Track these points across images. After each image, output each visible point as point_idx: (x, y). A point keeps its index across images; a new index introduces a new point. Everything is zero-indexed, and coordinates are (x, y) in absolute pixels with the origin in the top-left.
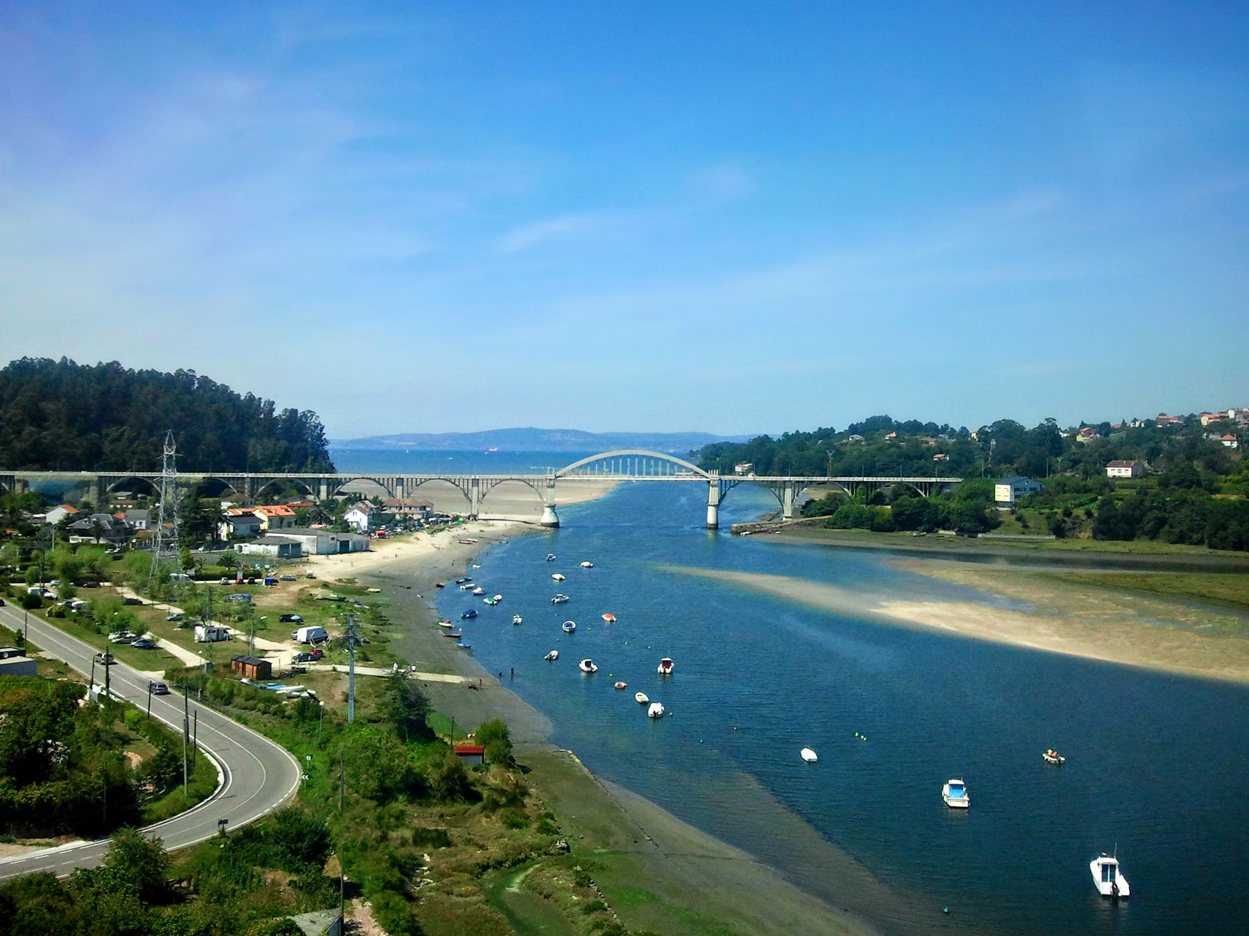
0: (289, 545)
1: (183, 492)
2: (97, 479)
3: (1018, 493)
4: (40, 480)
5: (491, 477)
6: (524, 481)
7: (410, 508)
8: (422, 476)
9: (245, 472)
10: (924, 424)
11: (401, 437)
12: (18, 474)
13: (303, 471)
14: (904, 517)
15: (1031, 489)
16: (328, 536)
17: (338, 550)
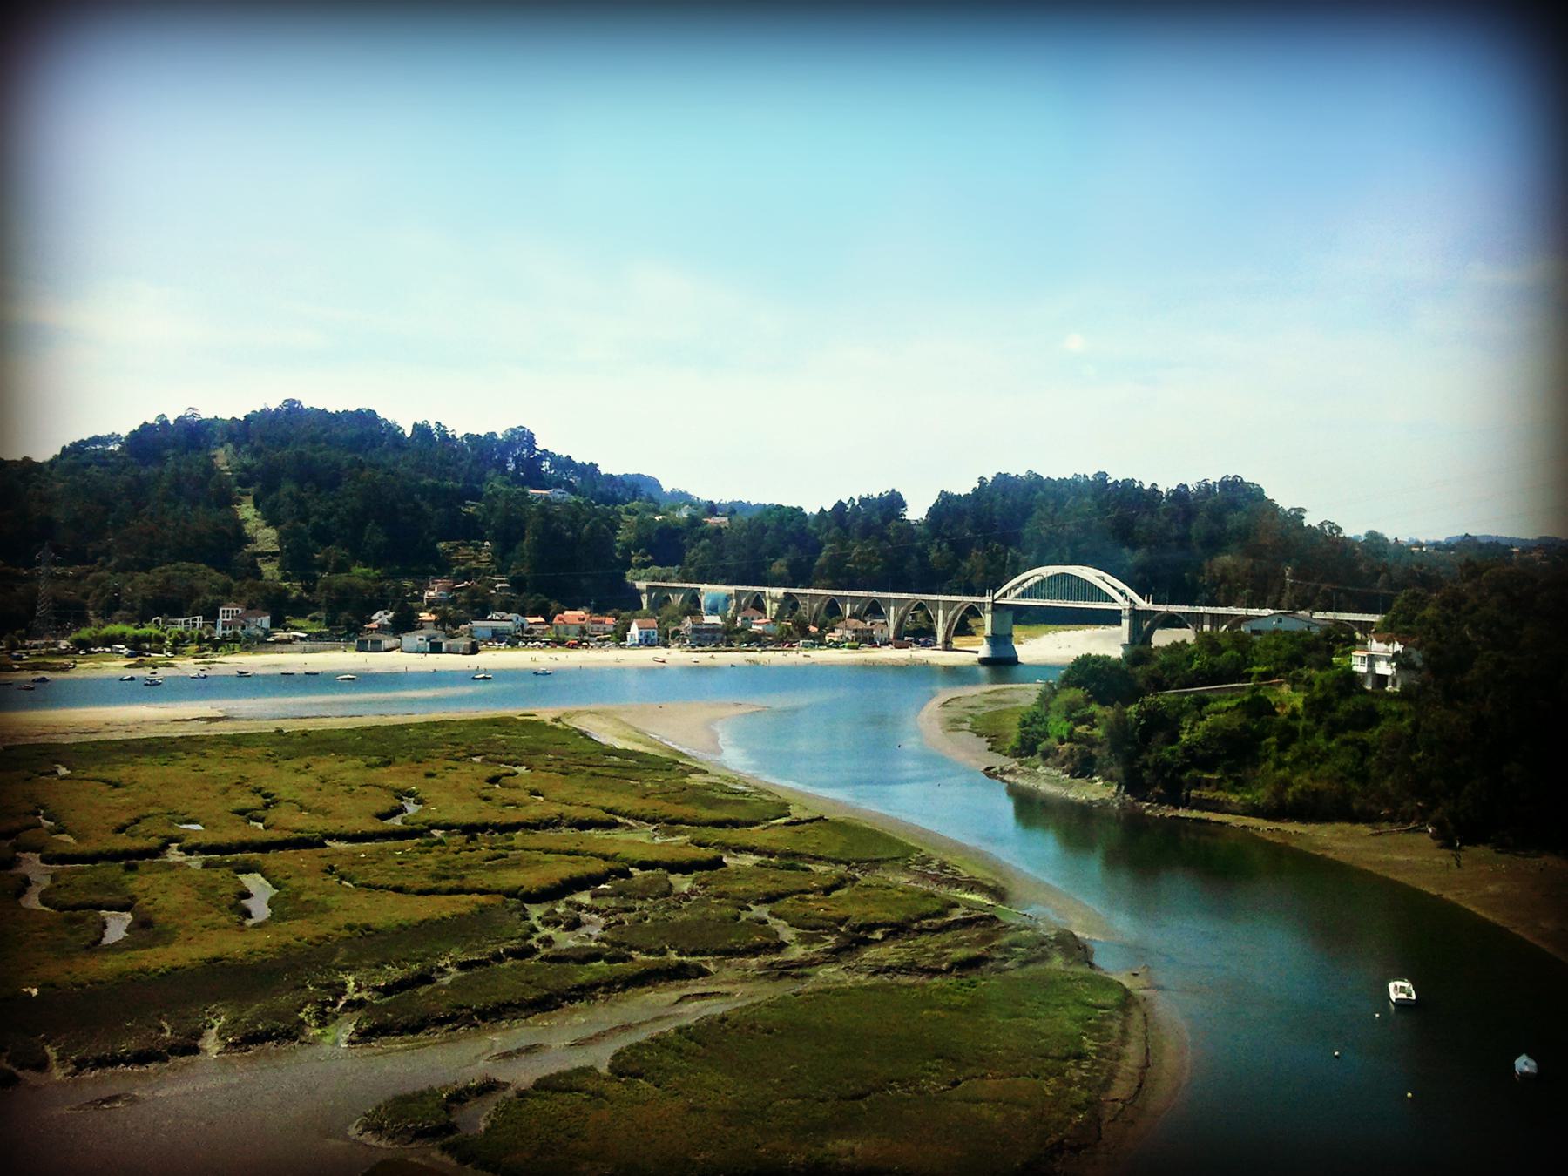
17: (428, 649)
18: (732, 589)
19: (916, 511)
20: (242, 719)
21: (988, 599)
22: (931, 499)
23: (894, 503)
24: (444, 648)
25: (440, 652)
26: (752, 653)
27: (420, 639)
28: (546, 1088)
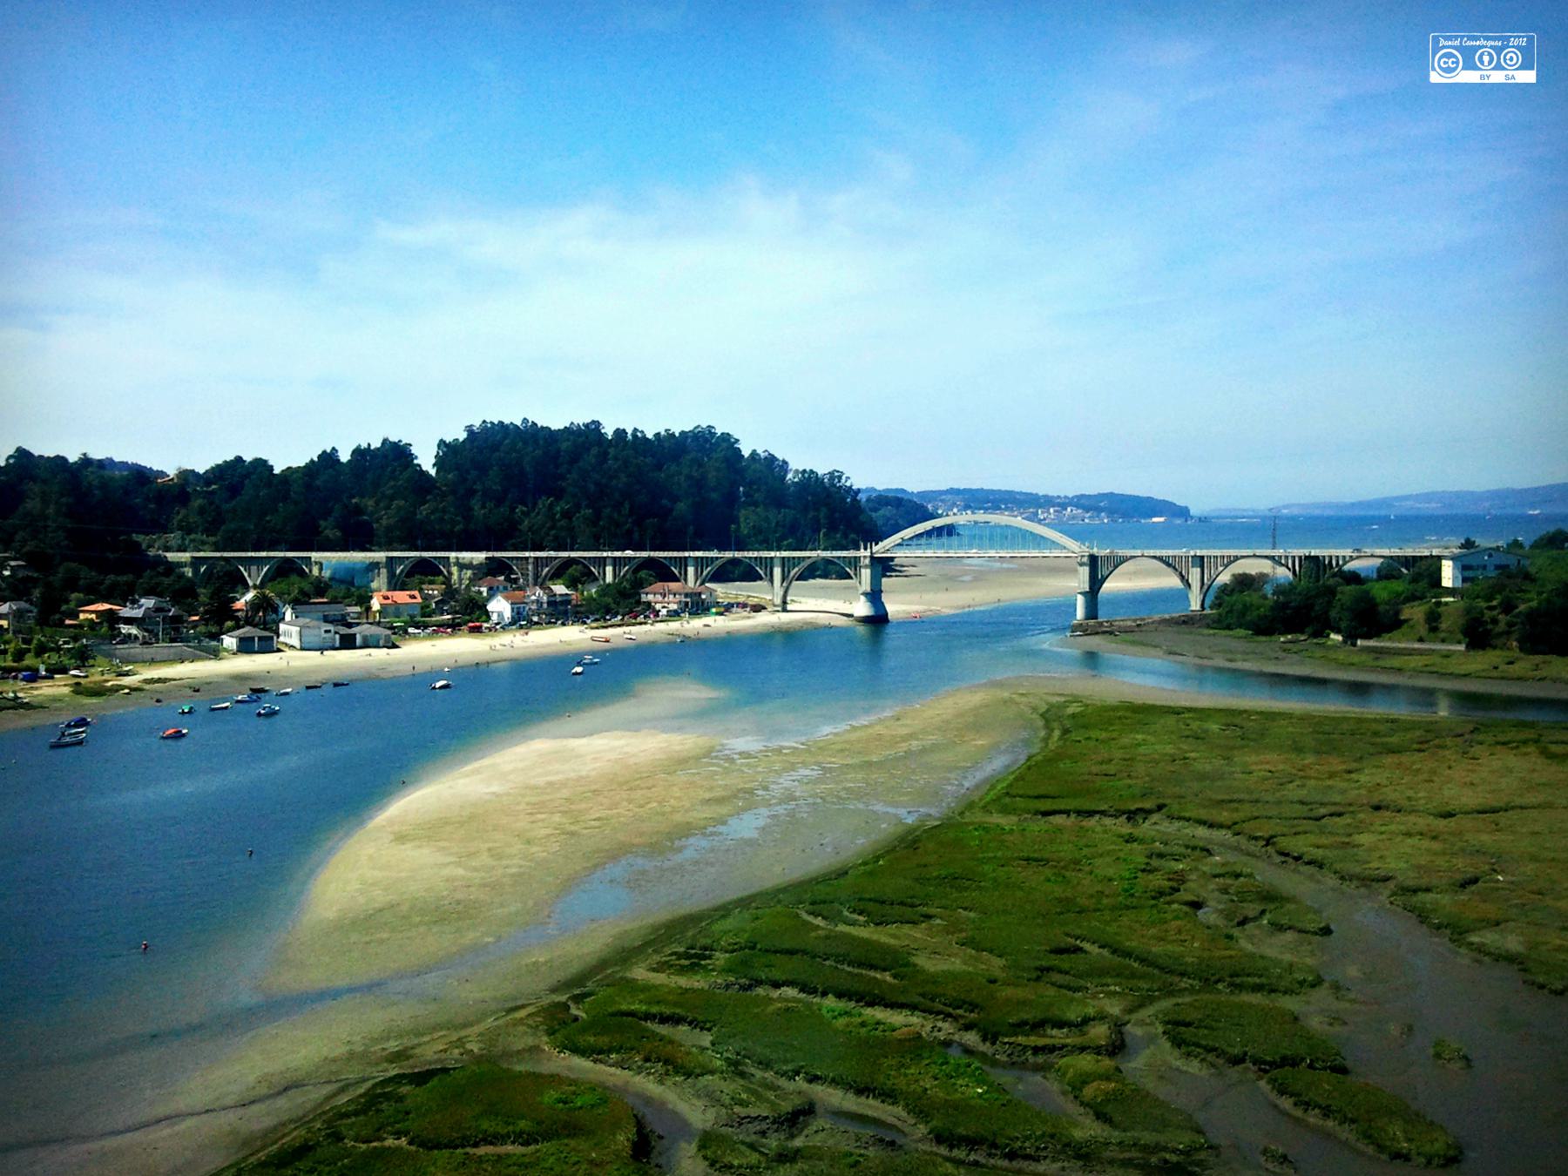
0: (253, 638)
1: (468, 575)
2: (384, 560)
3: (1470, 574)
4: (334, 561)
5: (1218, 553)
6: (1160, 559)
7: (675, 595)
8: (1226, 552)
9: (772, 550)
10: (277, 471)
11: (1428, 497)
12: (314, 555)
13: (810, 547)
14: (1288, 612)
15: (1497, 567)
16: (320, 628)
17: (337, 644)
18: (380, 556)
19: (316, 459)
20: (1485, 678)
21: (862, 553)
22: (750, 452)
23: (416, 457)
24: (359, 641)
25: (355, 647)
26: (643, 626)
27: (326, 631)
28: (84, 1137)
